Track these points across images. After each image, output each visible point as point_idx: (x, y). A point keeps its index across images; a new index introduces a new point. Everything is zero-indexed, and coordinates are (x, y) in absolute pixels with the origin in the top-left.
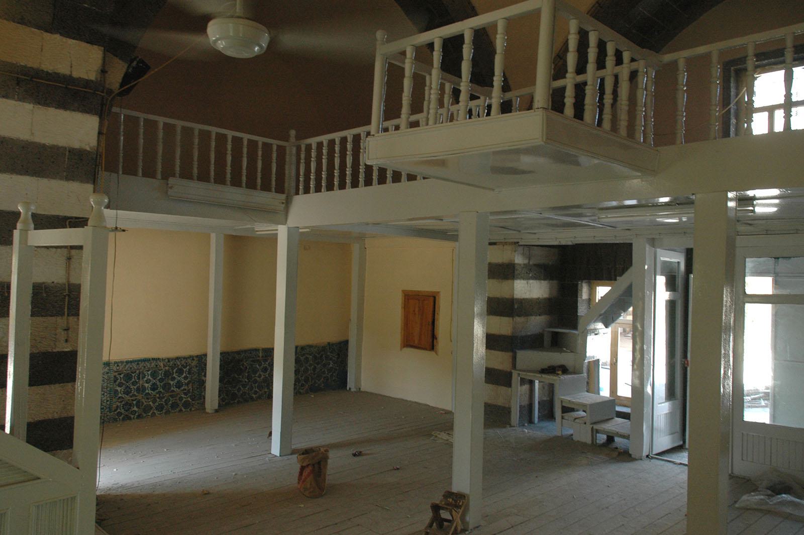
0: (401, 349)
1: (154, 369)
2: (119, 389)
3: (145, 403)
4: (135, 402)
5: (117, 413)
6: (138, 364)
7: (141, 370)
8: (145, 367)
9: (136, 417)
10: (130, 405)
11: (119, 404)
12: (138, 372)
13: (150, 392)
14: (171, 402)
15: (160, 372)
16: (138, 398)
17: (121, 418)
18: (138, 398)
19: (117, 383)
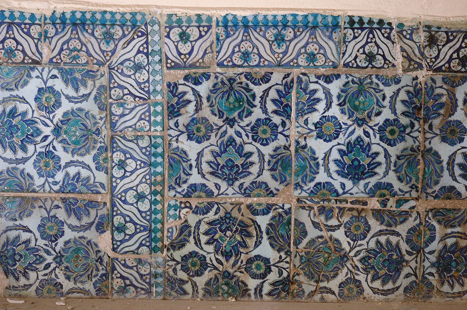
0: (316, 139)
1: (358, 74)
2: (192, 148)
3: (312, 233)
4: (263, 221)
5: (185, 258)
6: (279, 39)
7: (295, 72)
8: (312, 57)
9: (267, 288)
10: (244, 230)
11: (193, 220)
12: (277, 77)
13: (337, 182)
14: (435, 246)
15: (389, 91)
16: (277, 200)
17: (201, 281)
18: (277, 200)
19: (183, 120)
